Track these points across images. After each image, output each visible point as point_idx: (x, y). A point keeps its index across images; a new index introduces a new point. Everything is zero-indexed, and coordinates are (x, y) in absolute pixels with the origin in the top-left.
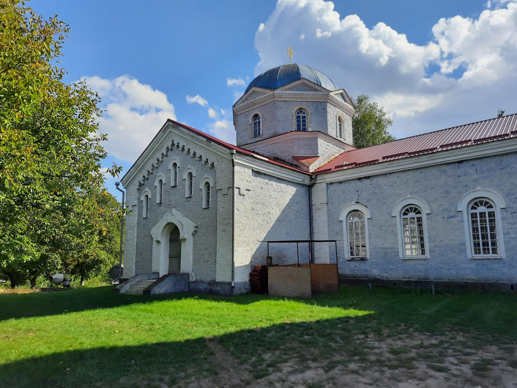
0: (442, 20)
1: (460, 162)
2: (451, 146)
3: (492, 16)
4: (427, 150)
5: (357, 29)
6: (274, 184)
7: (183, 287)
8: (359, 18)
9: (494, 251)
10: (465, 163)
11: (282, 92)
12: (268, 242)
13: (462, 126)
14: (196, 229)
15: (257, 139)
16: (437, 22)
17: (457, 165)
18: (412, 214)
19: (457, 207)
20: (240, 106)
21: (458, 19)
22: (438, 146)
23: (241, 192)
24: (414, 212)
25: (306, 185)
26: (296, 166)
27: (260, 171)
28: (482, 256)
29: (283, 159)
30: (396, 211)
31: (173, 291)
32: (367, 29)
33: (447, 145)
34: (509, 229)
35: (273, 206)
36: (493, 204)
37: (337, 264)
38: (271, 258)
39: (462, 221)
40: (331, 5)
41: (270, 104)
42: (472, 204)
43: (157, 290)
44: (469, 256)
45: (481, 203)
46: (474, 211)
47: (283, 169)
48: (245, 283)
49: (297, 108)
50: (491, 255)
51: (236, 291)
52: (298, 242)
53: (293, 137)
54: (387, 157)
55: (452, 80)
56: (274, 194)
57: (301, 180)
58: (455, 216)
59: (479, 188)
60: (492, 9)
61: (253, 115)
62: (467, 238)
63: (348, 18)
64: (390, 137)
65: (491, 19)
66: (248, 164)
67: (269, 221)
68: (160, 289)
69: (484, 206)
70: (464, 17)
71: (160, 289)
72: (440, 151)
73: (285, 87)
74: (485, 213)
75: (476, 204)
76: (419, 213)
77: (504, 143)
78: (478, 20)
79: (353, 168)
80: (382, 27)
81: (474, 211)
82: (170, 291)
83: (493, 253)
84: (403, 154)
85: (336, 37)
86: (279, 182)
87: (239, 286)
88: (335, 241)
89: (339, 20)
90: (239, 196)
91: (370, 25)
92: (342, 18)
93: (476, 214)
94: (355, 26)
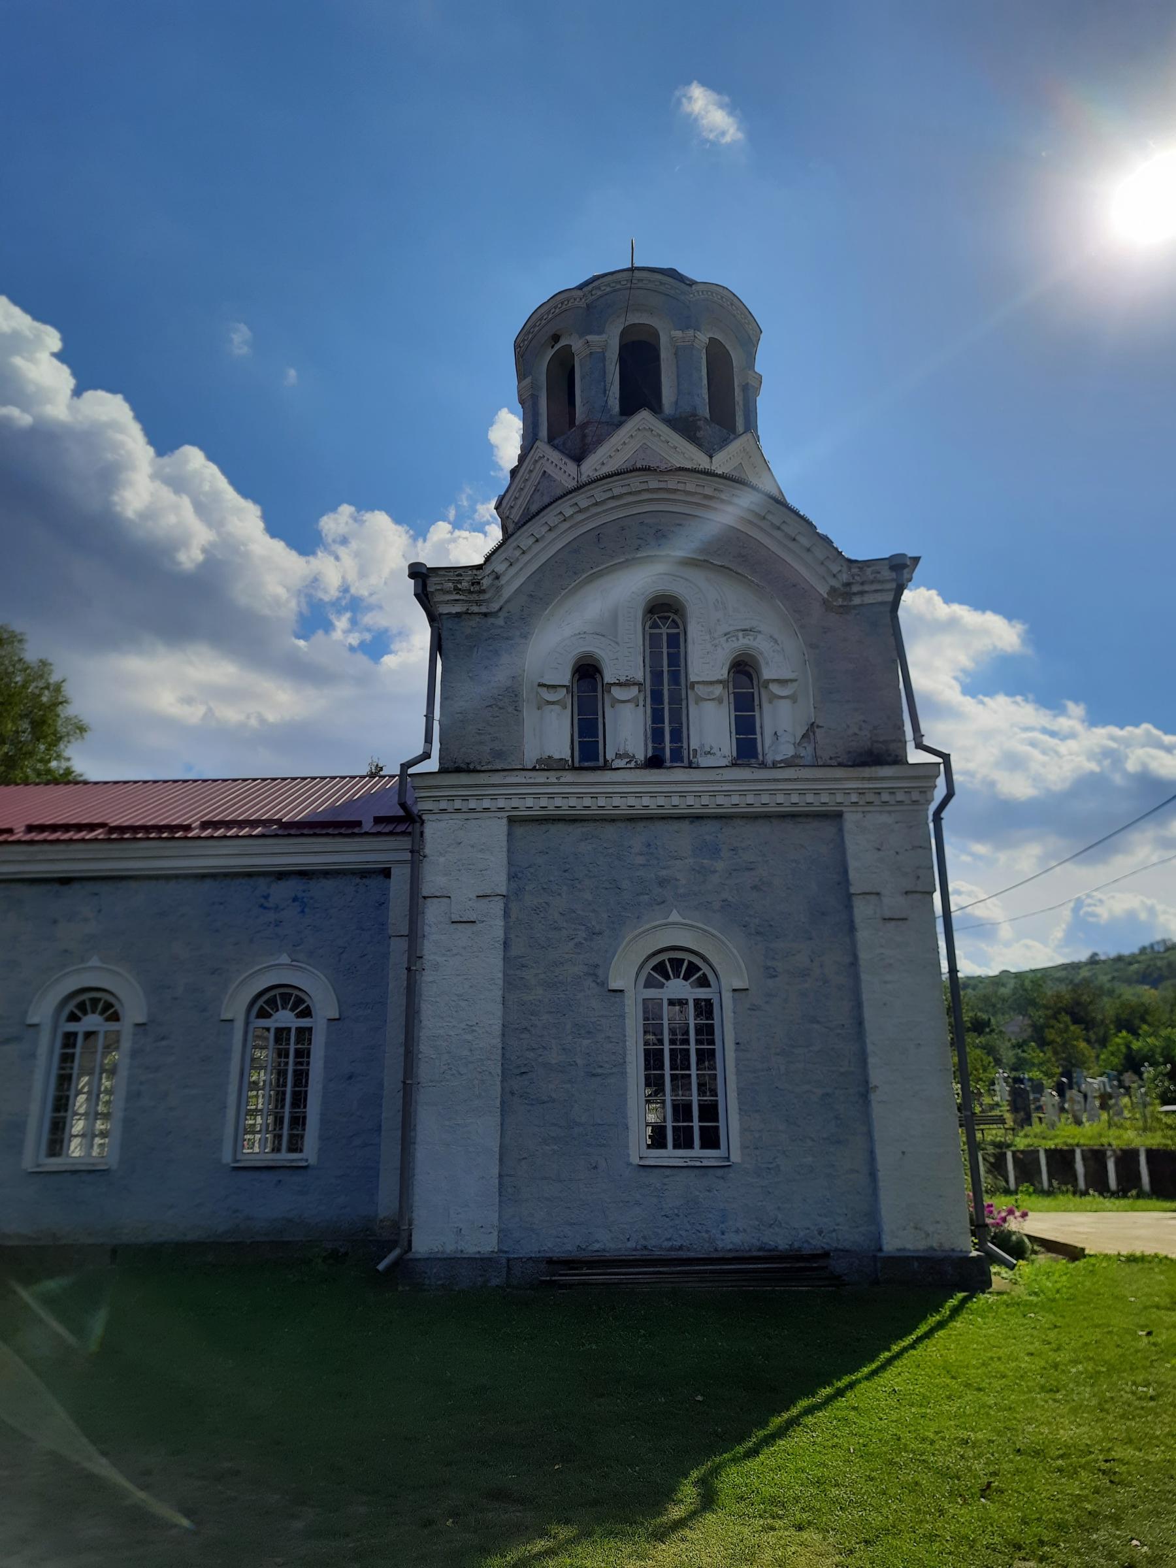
0: (346, 510)
1: (66, 881)
2: (298, 828)
3: (454, 540)
4: (160, 828)
5: (119, 437)
8: (130, 414)
9: (711, 1140)
10: (76, 886)
13: (315, 778)
16: (334, 508)
17: (56, 887)
18: (285, 1018)
19: (26, 1012)
21: (380, 520)
22: (195, 821)
24: (102, 1013)
28: (670, 1155)
30: (236, 1006)
32: (151, 451)
33: (216, 825)
34: (141, 1083)
36: (711, 977)
39: (33, 1056)
40: (53, 340)
42: (71, 1006)
44: (28, 1163)
45: (272, 1002)
46: (72, 1027)
50: (698, 1154)
54: (42, 828)
55: (362, 660)
58: (17, 1039)
59: (94, 962)
60: (457, 525)
62: (35, 1108)
63: (89, 395)
64: (68, 772)
65: (451, 546)
69: (93, 1012)
70: (397, 520)
72: (179, 838)
74: (289, 1029)
75: (272, 1002)
76: (115, 1017)
77: (172, 848)
78: (425, 541)
79: (95, 840)
80: (194, 458)
81: (72, 1027)
83: (676, 1147)
84: (92, 827)
85: (46, 435)
89: (69, 393)
91: (163, 440)
92: (77, 392)
93: (75, 1034)
94: (114, 425)
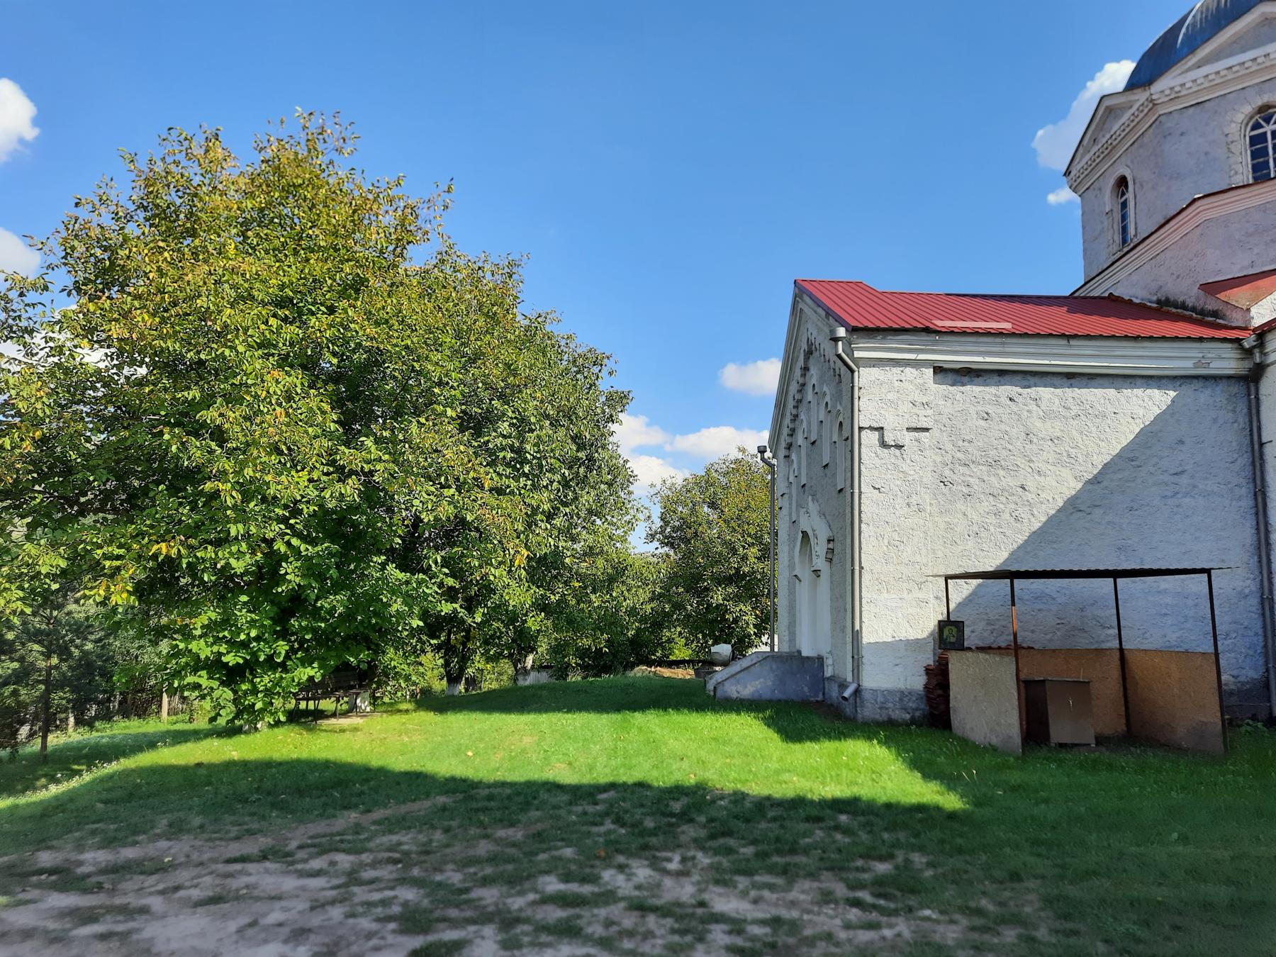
6: (1047, 394)
7: (806, 689)
11: (1180, 80)
12: (947, 578)
14: (831, 546)
15: (1126, 250)
20: (1079, 167)
23: (889, 439)
25: (1229, 377)
26: (1215, 314)
27: (945, 366)
29: (1181, 299)
31: (778, 695)
35: (1043, 467)
37: (1217, 654)
38: (959, 625)
41: (1151, 130)
43: (734, 688)
47: (1072, 342)
48: (903, 695)
49: (1248, 109)
51: (868, 711)
52: (1115, 574)
53: (1198, 220)
56: (1044, 428)
57: (1189, 364)
61: (1112, 181)
66: (912, 356)
67: (1023, 512)
68: (740, 688)
71: (740, 688)
73: (1193, 60)
82: (767, 695)
86: (1071, 386)
87: (880, 699)
88: (1208, 571)
90: (880, 451)
